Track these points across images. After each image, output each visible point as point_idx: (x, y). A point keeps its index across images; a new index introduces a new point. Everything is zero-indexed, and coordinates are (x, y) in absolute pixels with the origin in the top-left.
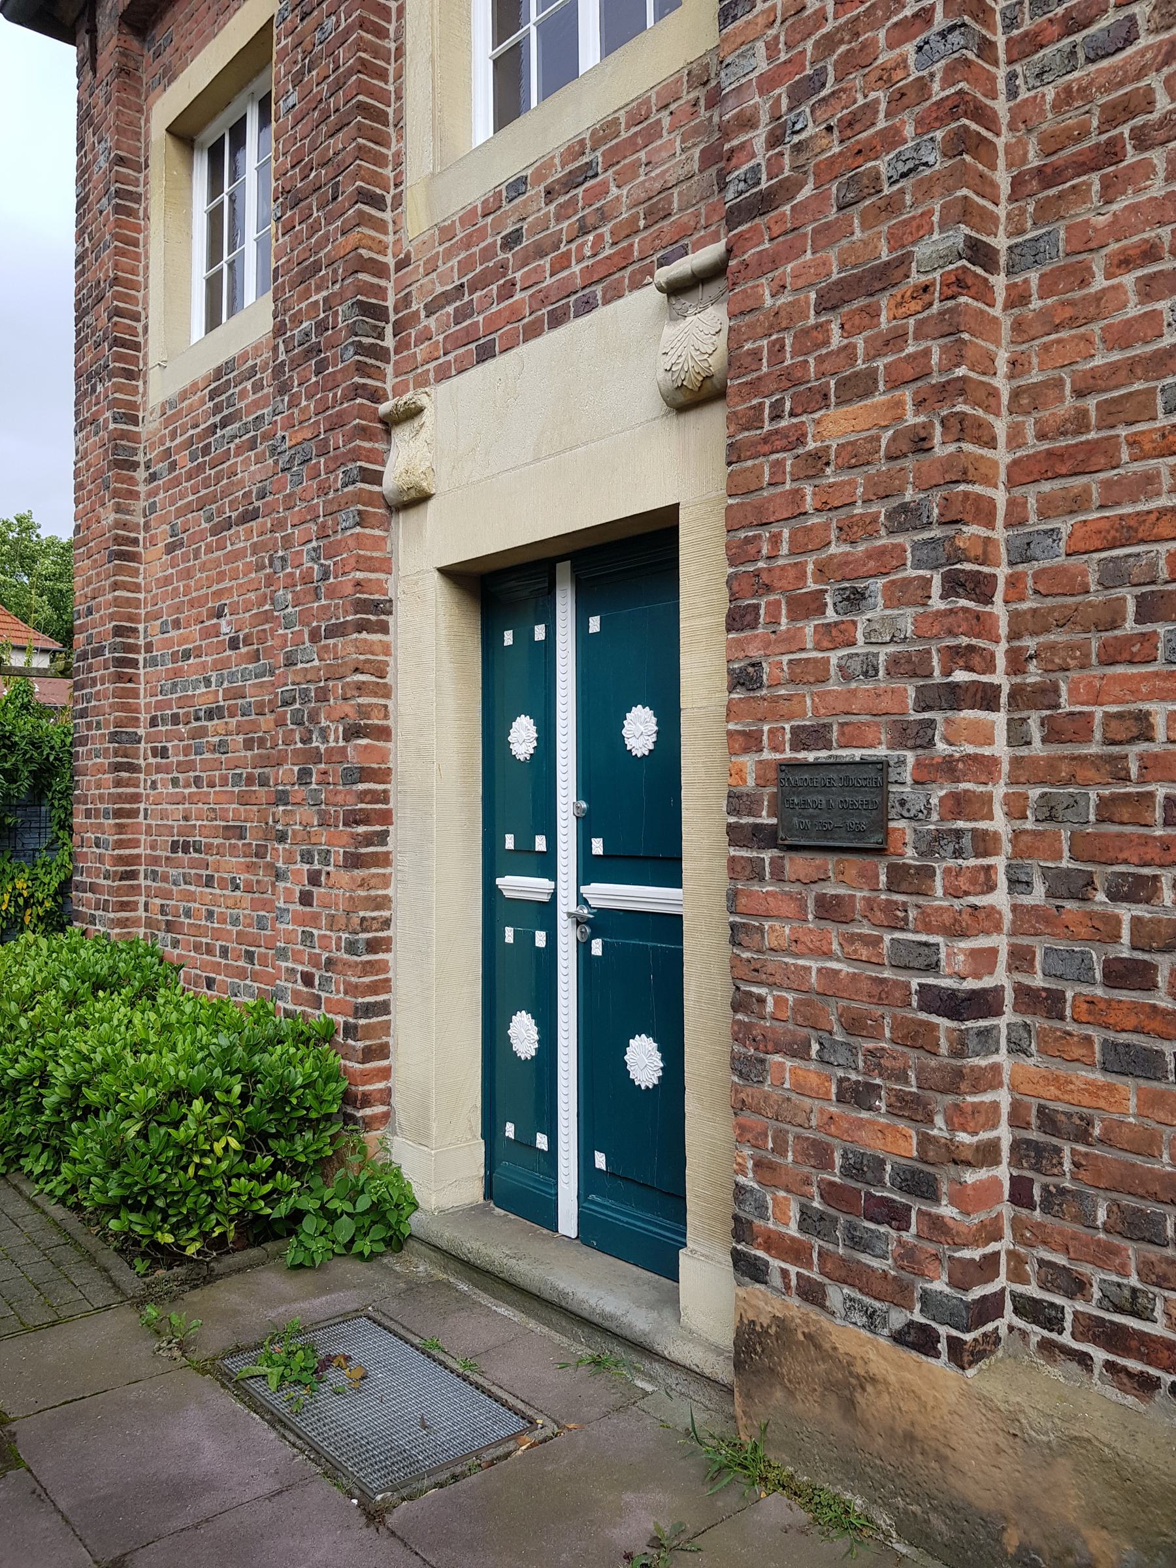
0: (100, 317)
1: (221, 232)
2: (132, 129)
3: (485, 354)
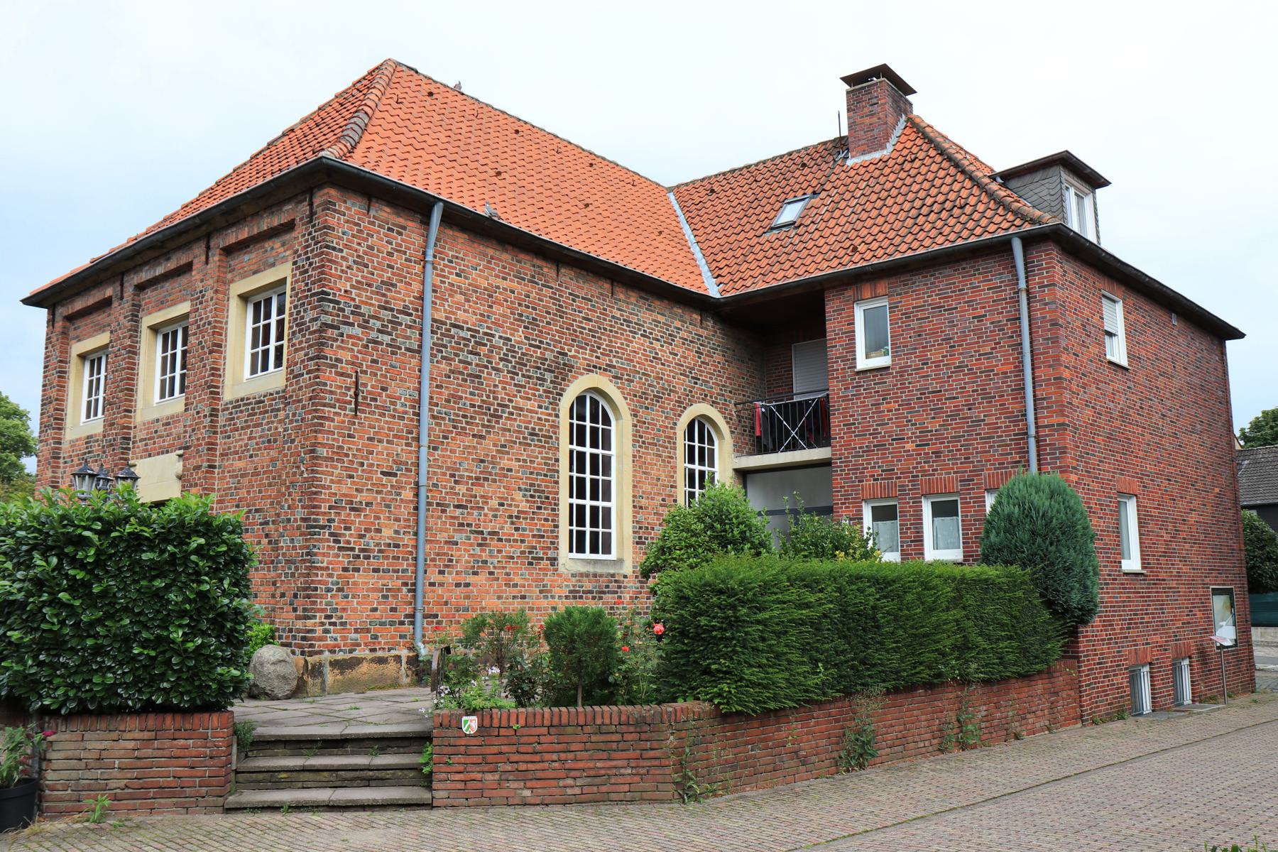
0: (51, 408)
1: (93, 388)
2: (65, 352)
3: (150, 455)
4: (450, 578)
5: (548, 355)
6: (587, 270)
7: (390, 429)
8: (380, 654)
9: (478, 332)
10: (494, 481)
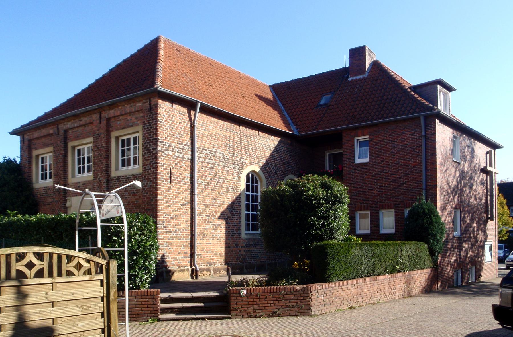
4: (204, 241)
5: (237, 159)
6: (250, 126)
7: (183, 188)
8: (182, 268)
9: (212, 151)
10: (219, 206)
